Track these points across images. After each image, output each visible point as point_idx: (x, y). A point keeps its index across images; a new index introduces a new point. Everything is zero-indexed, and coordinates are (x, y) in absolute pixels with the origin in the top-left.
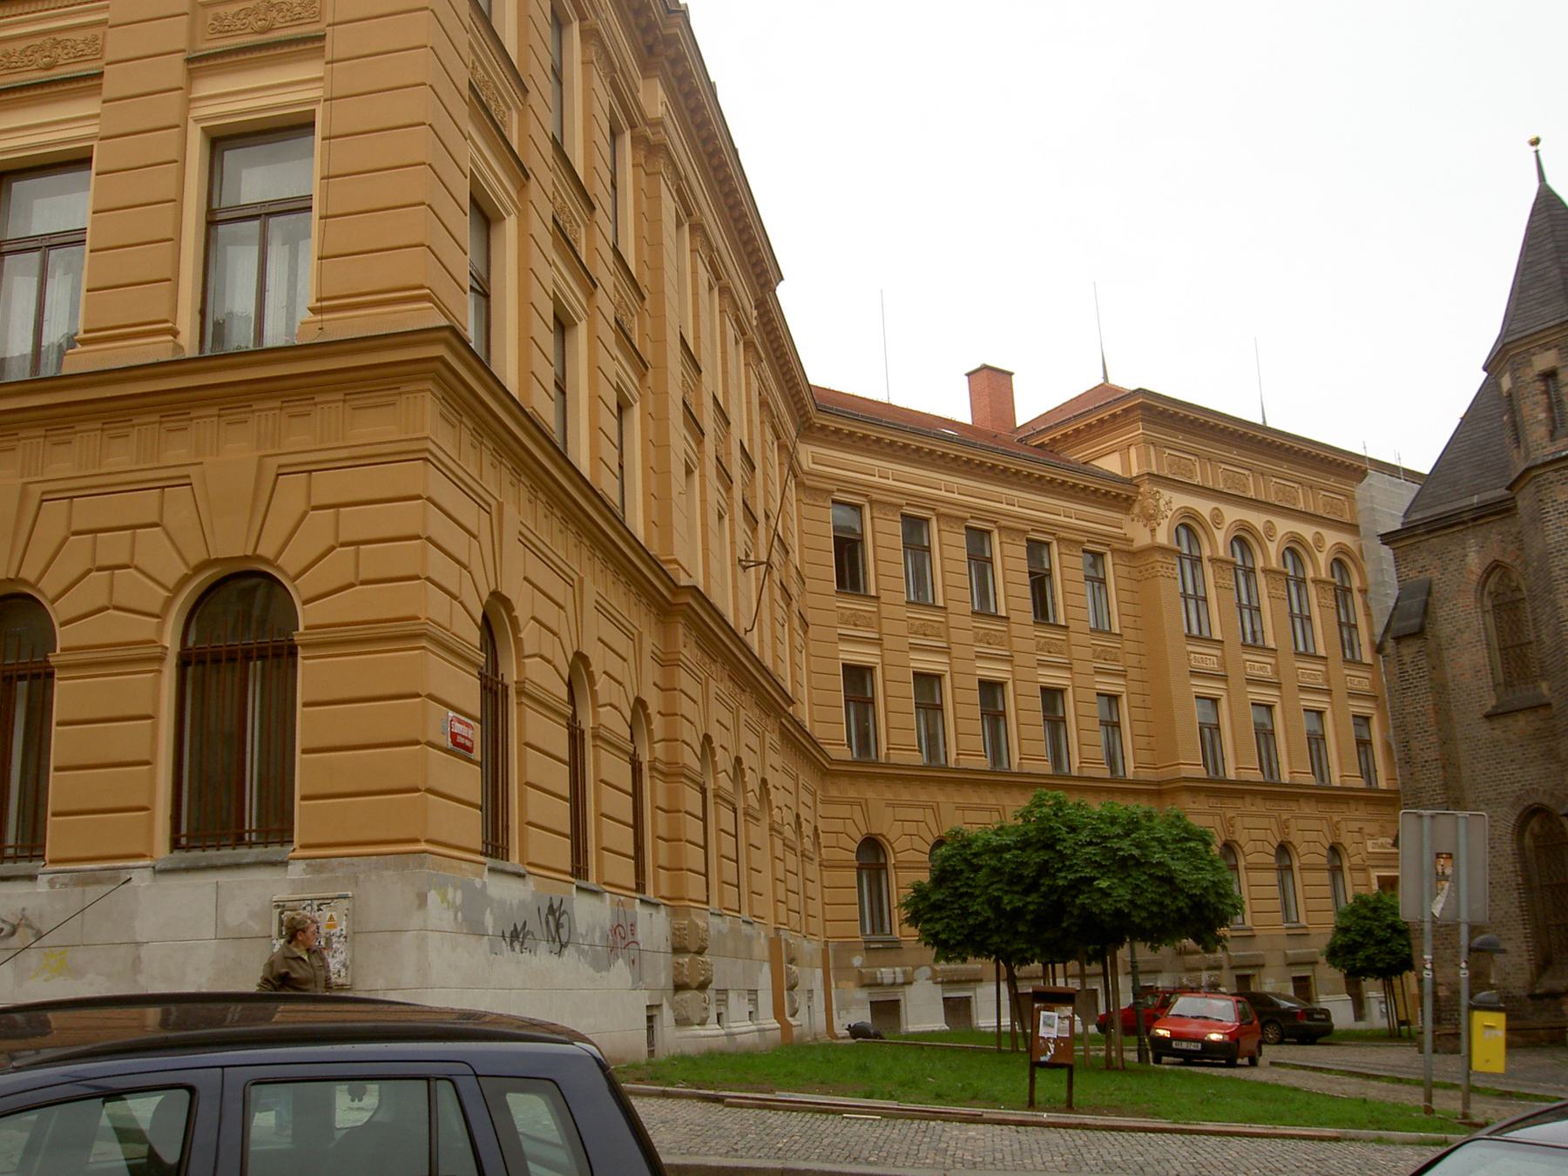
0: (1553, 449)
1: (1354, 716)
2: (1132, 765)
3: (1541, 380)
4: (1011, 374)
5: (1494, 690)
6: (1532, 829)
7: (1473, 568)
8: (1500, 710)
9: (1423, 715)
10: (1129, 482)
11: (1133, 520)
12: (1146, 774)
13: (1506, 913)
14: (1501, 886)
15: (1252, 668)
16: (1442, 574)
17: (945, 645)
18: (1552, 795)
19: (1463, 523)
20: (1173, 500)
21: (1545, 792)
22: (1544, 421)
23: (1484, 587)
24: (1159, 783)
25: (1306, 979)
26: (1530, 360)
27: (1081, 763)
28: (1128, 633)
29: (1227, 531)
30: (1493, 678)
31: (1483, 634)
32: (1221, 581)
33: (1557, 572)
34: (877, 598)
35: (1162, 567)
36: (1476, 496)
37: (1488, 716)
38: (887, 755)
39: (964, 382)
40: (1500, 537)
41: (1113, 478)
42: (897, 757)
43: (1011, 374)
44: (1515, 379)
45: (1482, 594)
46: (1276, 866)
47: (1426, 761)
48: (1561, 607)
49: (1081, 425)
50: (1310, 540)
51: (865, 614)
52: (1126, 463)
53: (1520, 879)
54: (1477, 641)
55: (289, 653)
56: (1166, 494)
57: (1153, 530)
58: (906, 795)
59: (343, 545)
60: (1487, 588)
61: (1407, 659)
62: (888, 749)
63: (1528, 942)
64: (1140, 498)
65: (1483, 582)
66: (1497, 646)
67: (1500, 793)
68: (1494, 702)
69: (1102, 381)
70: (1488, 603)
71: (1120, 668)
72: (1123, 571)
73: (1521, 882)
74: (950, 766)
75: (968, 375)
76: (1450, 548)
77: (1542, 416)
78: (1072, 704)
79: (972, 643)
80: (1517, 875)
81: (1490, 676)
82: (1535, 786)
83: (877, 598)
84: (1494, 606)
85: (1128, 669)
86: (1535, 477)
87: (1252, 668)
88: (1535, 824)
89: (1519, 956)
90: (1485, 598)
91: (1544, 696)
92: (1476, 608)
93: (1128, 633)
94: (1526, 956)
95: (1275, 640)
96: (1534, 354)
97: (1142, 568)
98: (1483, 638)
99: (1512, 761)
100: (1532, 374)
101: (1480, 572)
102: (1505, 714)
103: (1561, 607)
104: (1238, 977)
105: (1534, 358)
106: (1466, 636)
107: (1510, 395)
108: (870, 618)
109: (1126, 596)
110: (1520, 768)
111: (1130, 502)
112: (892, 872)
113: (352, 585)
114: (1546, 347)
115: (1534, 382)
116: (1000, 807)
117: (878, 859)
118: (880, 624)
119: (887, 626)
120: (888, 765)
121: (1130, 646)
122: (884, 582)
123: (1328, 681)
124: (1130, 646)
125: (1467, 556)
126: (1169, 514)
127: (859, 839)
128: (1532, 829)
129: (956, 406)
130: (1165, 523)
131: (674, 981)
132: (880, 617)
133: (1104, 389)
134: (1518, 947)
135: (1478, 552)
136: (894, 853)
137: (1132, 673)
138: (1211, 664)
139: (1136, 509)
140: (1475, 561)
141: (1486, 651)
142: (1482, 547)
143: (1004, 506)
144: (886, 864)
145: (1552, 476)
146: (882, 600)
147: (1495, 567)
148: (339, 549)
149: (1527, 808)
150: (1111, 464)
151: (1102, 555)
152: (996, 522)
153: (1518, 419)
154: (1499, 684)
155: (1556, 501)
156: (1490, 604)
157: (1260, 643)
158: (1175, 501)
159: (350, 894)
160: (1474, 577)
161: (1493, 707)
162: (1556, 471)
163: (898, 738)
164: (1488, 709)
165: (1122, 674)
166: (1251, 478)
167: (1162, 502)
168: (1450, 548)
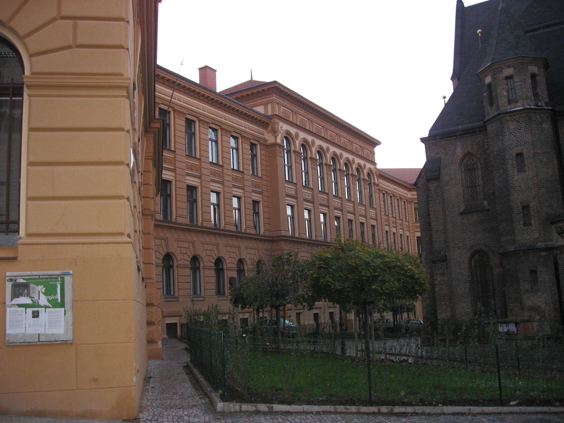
0: (509, 107)
1: (335, 216)
2: (263, 230)
3: (506, 79)
4: (216, 71)
5: (464, 203)
6: (475, 259)
7: (459, 155)
8: (467, 211)
9: (437, 211)
10: (268, 117)
11: (268, 133)
12: (267, 233)
13: (464, 292)
14: (462, 281)
15: (305, 195)
16: (445, 156)
17: (199, 175)
18: (486, 246)
19: (456, 136)
20: (283, 126)
21: (483, 244)
22: (506, 96)
23: (462, 162)
24: (273, 237)
25: (317, 314)
26: (502, 71)
27: (246, 227)
28: (264, 177)
29: (300, 141)
30: (464, 199)
31: (461, 181)
32: (297, 160)
33: (508, 156)
34: (174, 152)
35: (278, 152)
36: (460, 126)
37: (461, 214)
38: (176, 219)
39: (198, 72)
40: (471, 143)
41: (260, 114)
42: (180, 220)
43: (216, 71)
44: (494, 78)
45: (461, 165)
46: (237, 269)
47: (437, 230)
48: (509, 171)
49: (249, 93)
50: (325, 148)
51: (170, 158)
52: (266, 110)
53: (470, 278)
54: (458, 184)
55: (18, 91)
56: (281, 124)
57: (276, 137)
58: (182, 236)
59: (63, 18)
60: (463, 163)
61: (432, 189)
62: (176, 216)
63: (472, 303)
64: (271, 124)
65: (462, 160)
66: (465, 186)
67: (464, 244)
68: (464, 208)
69: (250, 79)
70: (463, 168)
71: (261, 191)
72: (263, 152)
73: (470, 280)
74: (198, 225)
75: (199, 69)
76: (450, 145)
77: (505, 94)
78: (243, 203)
79: (209, 175)
80: (469, 277)
81: (463, 198)
82: (479, 242)
83: (174, 152)
84: (465, 170)
85: (264, 191)
86: (501, 118)
87: (305, 195)
88: (476, 257)
89: (468, 309)
90: (462, 167)
91: (485, 207)
92: (459, 170)
93: (264, 177)
94: (471, 309)
95: (313, 185)
96: (503, 69)
97: (270, 152)
98: (461, 182)
99: (470, 232)
100: (502, 76)
101: (461, 156)
102: (468, 213)
103: (509, 171)
104: (297, 313)
105: (503, 70)
106: (453, 181)
107: (489, 85)
108: (171, 160)
109: (264, 163)
110: (474, 235)
111: (268, 125)
112: (225, 271)
113: (69, 47)
114: (509, 66)
115: (503, 80)
116: (217, 244)
117: (169, 263)
118: (175, 163)
119: (178, 164)
120: (176, 223)
121: (265, 183)
122: (178, 146)
123: (328, 202)
124: (265, 183)
125: (456, 149)
126: (282, 132)
127: (164, 254)
128: (475, 259)
129: (195, 78)
130: (280, 135)
131: (147, 321)
132: (175, 160)
133: (251, 81)
134: (468, 305)
135: (461, 148)
136: (177, 261)
137: (265, 193)
138: (292, 192)
139: (270, 129)
140: (459, 152)
141: (461, 188)
142: (463, 146)
143: (223, 120)
144: (173, 265)
145: (508, 118)
146: (177, 153)
147: (468, 154)
148: (60, 21)
149: (475, 251)
150: (260, 109)
151: (256, 145)
152: (220, 126)
153: (493, 94)
154: (466, 201)
155: (509, 128)
156: (463, 169)
157: (307, 186)
158: (284, 127)
159: (71, 272)
160: (459, 158)
161: (464, 210)
162: (510, 116)
163: (180, 212)
164: (462, 210)
165: (261, 193)
166: (308, 122)
167: (279, 127)
168: (450, 145)
